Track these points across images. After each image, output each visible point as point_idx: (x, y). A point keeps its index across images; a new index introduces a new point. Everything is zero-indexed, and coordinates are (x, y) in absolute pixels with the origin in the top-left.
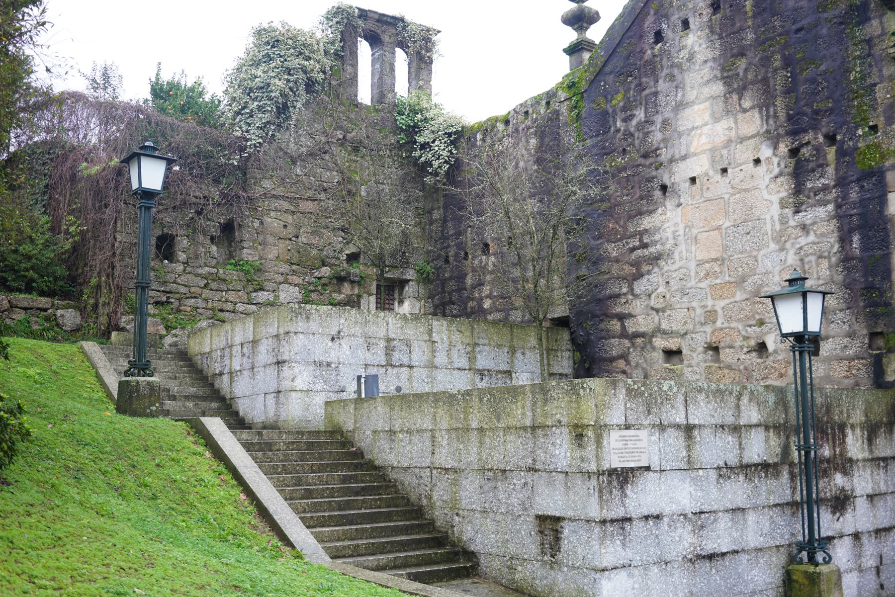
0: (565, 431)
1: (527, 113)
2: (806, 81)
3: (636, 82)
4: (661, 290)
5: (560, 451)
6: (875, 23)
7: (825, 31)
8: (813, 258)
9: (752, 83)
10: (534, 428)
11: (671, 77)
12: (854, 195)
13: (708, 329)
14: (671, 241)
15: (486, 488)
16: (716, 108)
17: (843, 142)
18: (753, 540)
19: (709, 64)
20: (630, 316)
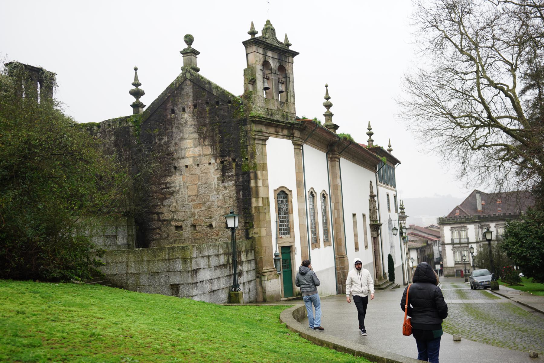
0: (180, 260)
1: (109, 125)
2: (227, 140)
3: (163, 126)
4: (174, 204)
5: (179, 265)
6: (248, 126)
7: (233, 125)
8: (228, 198)
9: (208, 136)
10: (169, 260)
11: (178, 128)
12: (241, 179)
13: (192, 219)
14: (178, 187)
15: (151, 278)
16: (195, 143)
17: (237, 162)
18: (222, 286)
19: (193, 126)
20: (162, 213)
